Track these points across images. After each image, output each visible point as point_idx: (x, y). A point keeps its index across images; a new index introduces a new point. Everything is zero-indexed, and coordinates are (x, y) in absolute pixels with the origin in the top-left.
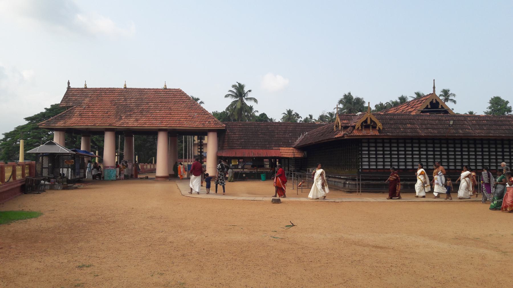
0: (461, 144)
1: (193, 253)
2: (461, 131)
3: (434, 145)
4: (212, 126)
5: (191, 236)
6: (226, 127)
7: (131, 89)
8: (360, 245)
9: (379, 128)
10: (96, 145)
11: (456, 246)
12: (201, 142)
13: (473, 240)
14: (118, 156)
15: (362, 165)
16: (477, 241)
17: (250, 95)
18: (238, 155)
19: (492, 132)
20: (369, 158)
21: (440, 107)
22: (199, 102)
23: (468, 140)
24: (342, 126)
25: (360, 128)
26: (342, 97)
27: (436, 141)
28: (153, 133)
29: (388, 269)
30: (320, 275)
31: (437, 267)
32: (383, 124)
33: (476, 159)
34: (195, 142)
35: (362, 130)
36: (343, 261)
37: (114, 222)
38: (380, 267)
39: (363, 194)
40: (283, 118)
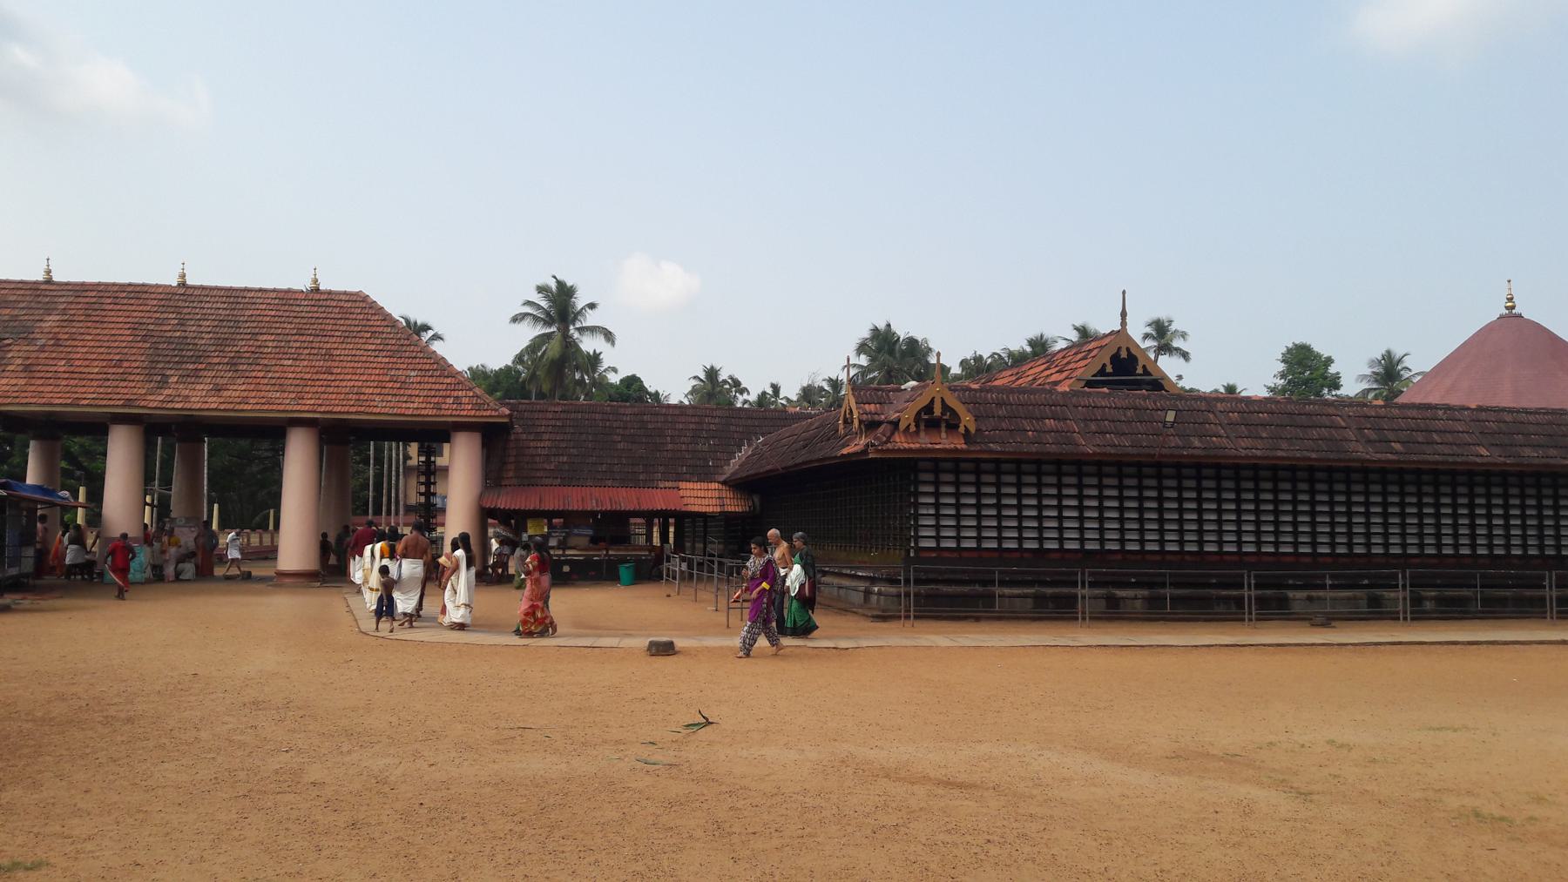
0: (1159, 477)
1: (385, 819)
2: (1197, 443)
3: (998, 478)
4: (467, 413)
5: (382, 762)
6: (510, 416)
7: (203, 288)
8: (899, 779)
9: (967, 429)
10: (80, 467)
11: (1174, 780)
12: (428, 463)
13: (1221, 759)
14: (151, 505)
15: (917, 538)
16: (1233, 763)
17: (591, 319)
18: (549, 505)
19: (1284, 445)
20: (937, 516)
21: (1140, 370)
22: (426, 336)
23: (1218, 467)
24: (860, 422)
25: (913, 428)
26: (866, 334)
27: (1086, 469)
28: (272, 433)
29: (978, 850)
30: (777, 873)
31: (1119, 843)
32: (977, 418)
33: (1239, 522)
34: (410, 463)
35: (917, 432)
36: (850, 829)
37: (130, 720)
38: (955, 844)
39: (918, 624)
40: (691, 393)
